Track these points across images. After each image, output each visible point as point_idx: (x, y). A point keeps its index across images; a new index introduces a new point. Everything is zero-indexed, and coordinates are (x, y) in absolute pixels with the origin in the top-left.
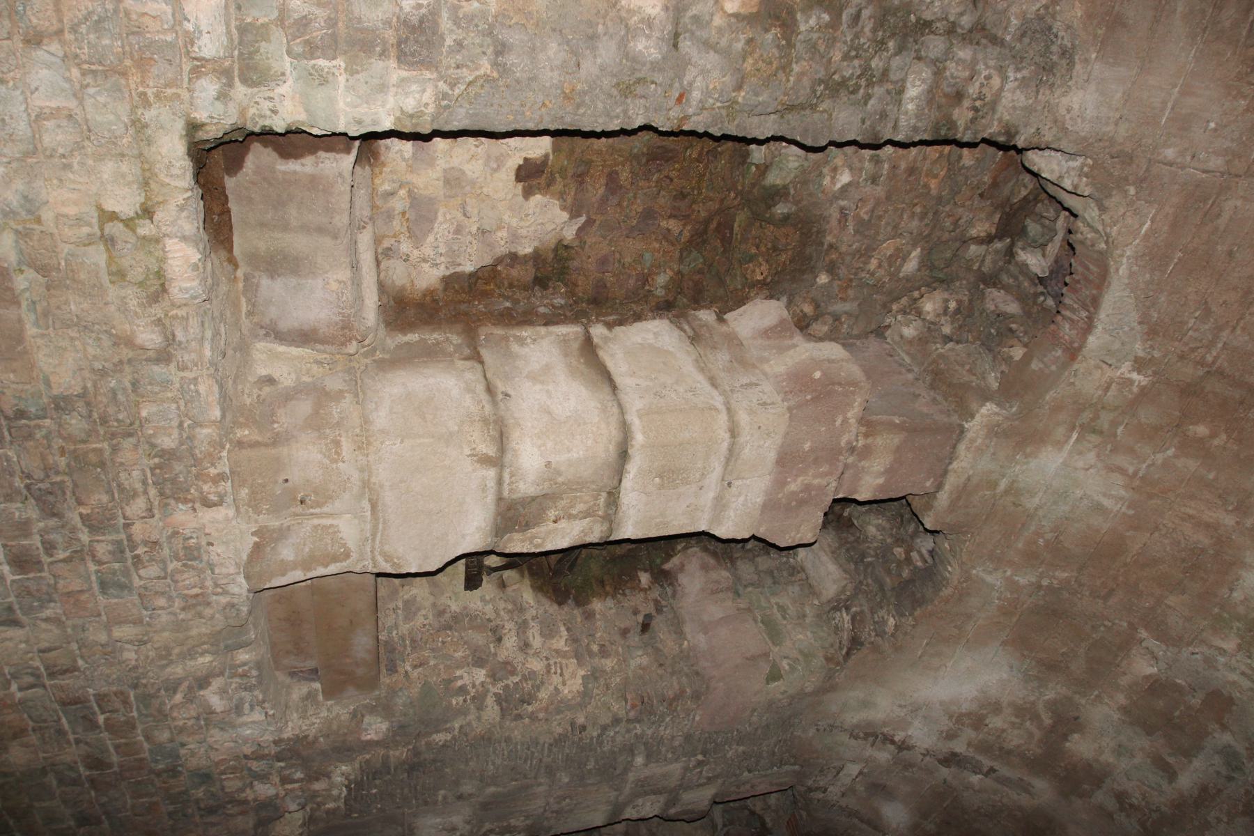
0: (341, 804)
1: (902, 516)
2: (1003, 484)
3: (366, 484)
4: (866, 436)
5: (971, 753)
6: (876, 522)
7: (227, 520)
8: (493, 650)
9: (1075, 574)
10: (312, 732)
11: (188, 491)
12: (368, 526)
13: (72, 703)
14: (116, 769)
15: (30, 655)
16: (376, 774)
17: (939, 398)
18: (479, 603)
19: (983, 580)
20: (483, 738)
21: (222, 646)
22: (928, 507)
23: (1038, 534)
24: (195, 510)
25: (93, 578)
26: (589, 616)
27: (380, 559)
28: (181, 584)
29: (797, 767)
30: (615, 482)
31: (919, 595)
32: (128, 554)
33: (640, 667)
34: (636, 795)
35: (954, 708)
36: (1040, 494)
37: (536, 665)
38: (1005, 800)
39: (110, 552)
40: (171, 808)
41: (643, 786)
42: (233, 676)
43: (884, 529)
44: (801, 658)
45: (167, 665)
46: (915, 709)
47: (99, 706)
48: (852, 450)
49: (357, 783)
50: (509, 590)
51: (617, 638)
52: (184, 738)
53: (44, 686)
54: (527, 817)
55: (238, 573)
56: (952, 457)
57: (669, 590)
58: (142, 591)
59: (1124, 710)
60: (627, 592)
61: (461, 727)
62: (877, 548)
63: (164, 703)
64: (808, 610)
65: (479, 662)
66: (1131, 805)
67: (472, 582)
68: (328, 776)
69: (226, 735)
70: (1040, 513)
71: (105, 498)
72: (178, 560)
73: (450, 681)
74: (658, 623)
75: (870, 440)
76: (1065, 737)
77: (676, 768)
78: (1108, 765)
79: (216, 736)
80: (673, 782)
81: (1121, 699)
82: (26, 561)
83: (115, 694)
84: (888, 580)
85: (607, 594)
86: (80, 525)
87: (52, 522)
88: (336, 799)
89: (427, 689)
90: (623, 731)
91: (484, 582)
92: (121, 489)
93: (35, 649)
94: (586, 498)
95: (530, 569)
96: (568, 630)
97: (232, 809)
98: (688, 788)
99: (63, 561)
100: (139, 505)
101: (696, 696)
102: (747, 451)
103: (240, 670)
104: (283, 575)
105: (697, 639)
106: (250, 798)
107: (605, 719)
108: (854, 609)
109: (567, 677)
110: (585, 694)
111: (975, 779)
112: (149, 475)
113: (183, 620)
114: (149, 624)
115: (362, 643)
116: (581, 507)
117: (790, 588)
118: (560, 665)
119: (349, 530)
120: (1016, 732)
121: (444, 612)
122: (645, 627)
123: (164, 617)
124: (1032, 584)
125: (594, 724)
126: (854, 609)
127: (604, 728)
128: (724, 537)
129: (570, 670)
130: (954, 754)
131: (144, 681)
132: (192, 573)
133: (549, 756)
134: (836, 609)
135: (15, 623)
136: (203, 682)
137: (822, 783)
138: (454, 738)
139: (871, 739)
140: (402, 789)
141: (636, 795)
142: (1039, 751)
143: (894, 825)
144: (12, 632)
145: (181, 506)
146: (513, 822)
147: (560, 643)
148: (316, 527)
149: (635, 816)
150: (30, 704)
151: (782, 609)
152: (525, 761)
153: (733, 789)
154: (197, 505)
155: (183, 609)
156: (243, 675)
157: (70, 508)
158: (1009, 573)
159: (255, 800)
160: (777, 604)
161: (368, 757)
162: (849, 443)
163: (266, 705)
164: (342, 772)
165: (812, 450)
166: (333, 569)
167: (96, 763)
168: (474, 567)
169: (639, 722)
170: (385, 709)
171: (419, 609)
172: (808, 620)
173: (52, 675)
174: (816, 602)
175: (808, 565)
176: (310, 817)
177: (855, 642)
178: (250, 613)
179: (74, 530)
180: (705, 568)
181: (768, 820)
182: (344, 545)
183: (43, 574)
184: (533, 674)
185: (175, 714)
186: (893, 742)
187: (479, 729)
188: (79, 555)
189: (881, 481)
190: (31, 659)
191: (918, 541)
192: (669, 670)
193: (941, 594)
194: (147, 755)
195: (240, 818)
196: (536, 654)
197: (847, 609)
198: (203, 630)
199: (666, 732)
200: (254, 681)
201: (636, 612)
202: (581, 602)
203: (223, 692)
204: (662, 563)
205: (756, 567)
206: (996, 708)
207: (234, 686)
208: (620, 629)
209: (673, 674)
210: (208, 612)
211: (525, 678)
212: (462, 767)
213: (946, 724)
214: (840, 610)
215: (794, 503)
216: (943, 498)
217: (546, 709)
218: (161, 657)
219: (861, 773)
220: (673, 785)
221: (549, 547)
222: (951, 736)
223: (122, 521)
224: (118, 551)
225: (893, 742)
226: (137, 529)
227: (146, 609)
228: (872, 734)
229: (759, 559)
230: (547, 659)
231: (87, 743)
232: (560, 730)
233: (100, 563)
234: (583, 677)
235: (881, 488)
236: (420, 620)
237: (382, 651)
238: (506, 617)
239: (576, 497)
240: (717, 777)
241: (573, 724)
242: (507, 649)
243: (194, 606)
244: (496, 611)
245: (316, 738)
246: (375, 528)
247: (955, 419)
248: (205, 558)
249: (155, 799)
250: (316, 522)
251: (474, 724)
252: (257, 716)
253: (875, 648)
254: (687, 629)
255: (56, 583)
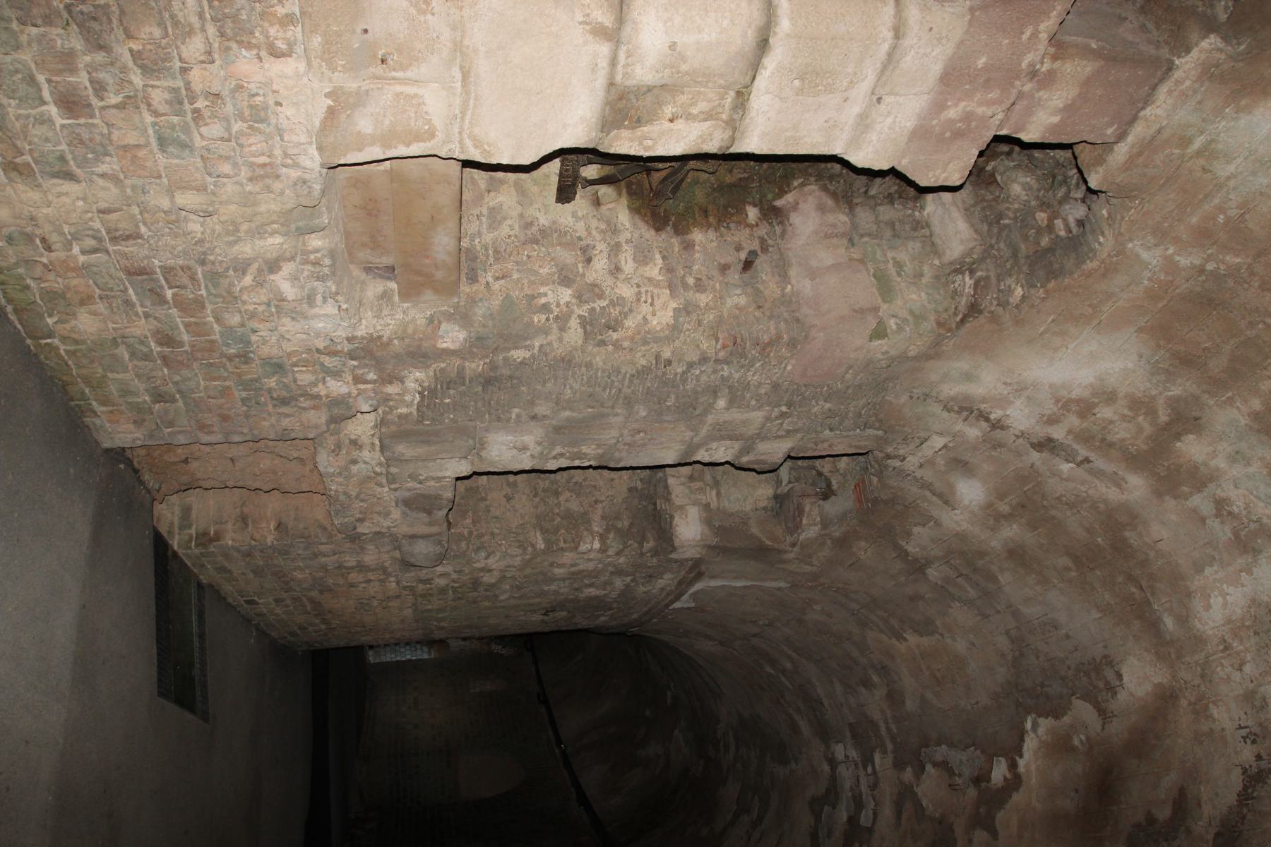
0: (414, 410)
1: (1054, 177)
2: (1198, 143)
3: (458, 47)
4: (1055, 58)
5: (1069, 441)
6: (1023, 180)
7: (298, 76)
8: (581, 270)
9: (1249, 260)
10: (386, 334)
11: (252, 33)
12: (458, 101)
13: (137, 273)
14: (187, 348)
15: (90, 215)
16: (449, 384)
17: (1150, 26)
18: (570, 219)
19: (1137, 256)
20: (563, 359)
21: (293, 227)
22: (1100, 161)
23: (1221, 209)
24: (260, 58)
25: (151, 131)
26: (688, 246)
27: (468, 143)
28: (246, 150)
29: (880, 433)
30: (748, 79)
31: (1057, 266)
32: (187, 107)
33: (737, 307)
34: (711, 438)
35: (1064, 393)
36: (1239, 160)
37: (626, 292)
38: (1091, 492)
39: (167, 102)
40: (244, 394)
41: (719, 430)
42: (306, 262)
43: (1030, 189)
44: (910, 319)
45: (235, 242)
46: (1021, 389)
47: (166, 279)
48: (1033, 74)
49: (430, 391)
50: (603, 208)
51: (715, 273)
52: (255, 325)
53: (107, 252)
54: (599, 446)
55: (311, 143)
56: (1147, 101)
57: (778, 229)
58: (205, 153)
59: (1256, 416)
60: (732, 225)
61: (541, 346)
62: (1017, 210)
63: (232, 284)
64: (926, 269)
65: (566, 281)
66: (1230, 513)
67: (565, 193)
68: (401, 380)
69: (298, 326)
70: (1232, 184)
71: (157, 32)
72: (243, 120)
73: (533, 297)
74: (762, 263)
75: (1057, 64)
76: (1178, 436)
77: (757, 416)
78: (1218, 469)
79: (287, 325)
80: (751, 431)
81: (1256, 404)
82: (74, 103)
83: (182, 268)
84: (1023, 246)
85: (709, 226)
86: (131, 64)
87: (100, 57)
88: (409, 405)
89: (508, 302)
90: (710, 370)
91: (578, 196)
92: (176, 24)
93: (94, 207)
94: (711, 95)
95: (629, 187)
96: (664, 258)
97: (304, 403)
98: (764, 438)
99: (116, 106)
100: (193, 48)
101: (792, 344)
102: (908, 58)
103: (312, 257)
104: (360, 150)
105: (801, 284)
106: (322, 393)
107: (693, 356)
108: (979, 274)
109: (657, 307)
110: (675, 328)
111: (1066, 467)
112: (206, 8)
113: (251, 193)
114: (214, 194)
115: (442, 243)
116: (703, 106)
117: (911, 244)
118: (653, 292)
119: (436, 103)
120: (1124, 425)
121: (531, 224)
122: (748, 265)
123: (230, 188)
124: (1193, 267)
125: (680, 361)
126: (979, 274)
127: (691, 365)
128: (860, 165)
129: (662, 300)
130: (1050, 440)
131: (212, 258)
132: (260, 137)
133: (629, 387)
134: (959, 271)
135: (69, 176)
136: (273, 266)
137: (901, 452)
138: (533, 356)
139: (965, 414)
140: (476, 402)
141: (711, 438)
142: (1145, 447)
143: (966, 502)
144: (67, 186)
145: (244, 52)
146: (584, 449)
147: (654, 270)
148: (398, 95)
149: (707, 459)
150: (95, 269)
151: (899, 265)
152: (604, 390)
153: (811, 445)
154: (263, 53)
155: (250, 179)
156: (316, 263)
157: (118, 41)
158: (1170, 251)
159: (327, 396)
160: (894, 259)
161: (443, 365)
162: (1032, 65)
163: (339, 298)
164: (416, 378)
165: (986, 68)
166: (415, 149)
167: (167, 340)
168: (573, 166)
169: (728, 363)
170: (462, 317)
171: (505, 218)
172: (924, 281)
173: (114, 240)
174: (937, 262)
175: (935, 222)
176: (382, 421)
177: (974, 309)
178: (323, 192)
179: (124, 69)
180: (821, 208)
181: (834, 482)
182: (429, 122)
183: (95, 121)
184: (620, 301)
185: (245, 297)
186: (987, 420)
187: (560, 350)
188: (131, 102)
189: (1056, 119)
190: (91, 219)
191: (1067, 207)
192: (768, 314)
193: (1084, 267)
194: (217, 337)
195: (313, 412)
196: (627, 280)
197: (972, 272)
198: (273, 207)
199: (753, 378)
200: (326, 270)
201: (738, 248)
202: (680, 230)
203: (294, 278)
204: (774, 199)
205: (877, 217)
206: (1110, 397)
207: (306, 273)
208: (720, 264)
209: (771, 318)
210: (277, 186)
211: (612, 303)
212: (539, 387)
213: (1050, 407)
214: (963, 273)
215: (948, 134)
216: (1121, 151)
217: (632, 339)
218: (228, 233)
219: (945, 446)
220: (750, 433)
221: (660, 151)
222: (1052, 421)
223: (179, 64)
224: (176, 102)
225: (987, 420)
226: (195, 74)
227: (210, 175)
228: (967, 409)
229: (881, 209)
230: (638, 286)
231: (156, 318)
232: (643, 362)
233: (156, 113)
234: (675, 309)
235: (1053, 129)
236: (505, 230)
237: (463, 259)
238: (598, 237)
239: (699, 93)
240: (796, 431)
241: (658, 357)
242: (596, 271)
243: (262, 177)
244: (588, 230)
245: (390, 340)
246: (465, 104)
247: (1165, 52)
248: (273, 121)
249: (227, 383)
250: (399, 88)
251: (555, 345)
252: (330, 309)
253: (994, 318)
254: (793, 273)
255: (110, 133)
